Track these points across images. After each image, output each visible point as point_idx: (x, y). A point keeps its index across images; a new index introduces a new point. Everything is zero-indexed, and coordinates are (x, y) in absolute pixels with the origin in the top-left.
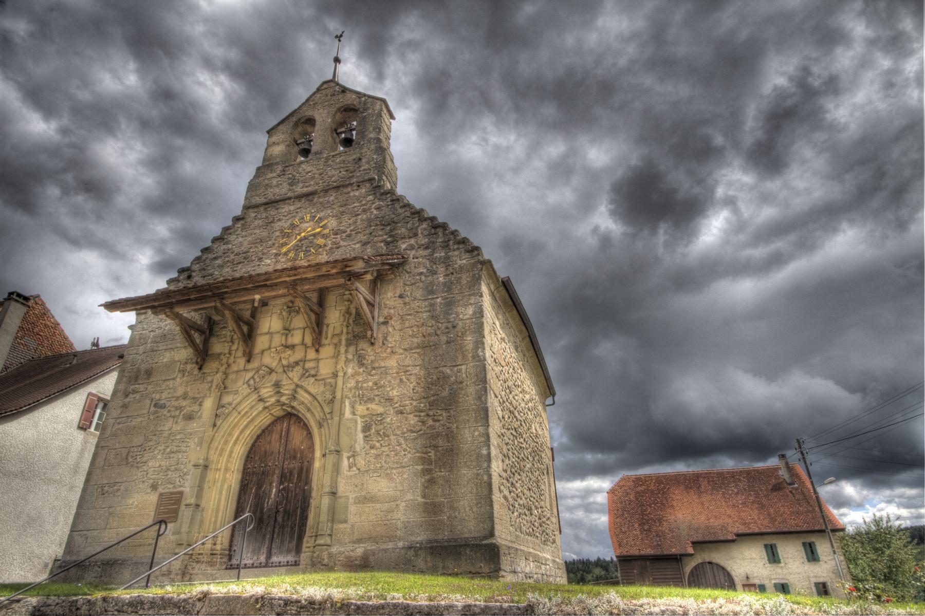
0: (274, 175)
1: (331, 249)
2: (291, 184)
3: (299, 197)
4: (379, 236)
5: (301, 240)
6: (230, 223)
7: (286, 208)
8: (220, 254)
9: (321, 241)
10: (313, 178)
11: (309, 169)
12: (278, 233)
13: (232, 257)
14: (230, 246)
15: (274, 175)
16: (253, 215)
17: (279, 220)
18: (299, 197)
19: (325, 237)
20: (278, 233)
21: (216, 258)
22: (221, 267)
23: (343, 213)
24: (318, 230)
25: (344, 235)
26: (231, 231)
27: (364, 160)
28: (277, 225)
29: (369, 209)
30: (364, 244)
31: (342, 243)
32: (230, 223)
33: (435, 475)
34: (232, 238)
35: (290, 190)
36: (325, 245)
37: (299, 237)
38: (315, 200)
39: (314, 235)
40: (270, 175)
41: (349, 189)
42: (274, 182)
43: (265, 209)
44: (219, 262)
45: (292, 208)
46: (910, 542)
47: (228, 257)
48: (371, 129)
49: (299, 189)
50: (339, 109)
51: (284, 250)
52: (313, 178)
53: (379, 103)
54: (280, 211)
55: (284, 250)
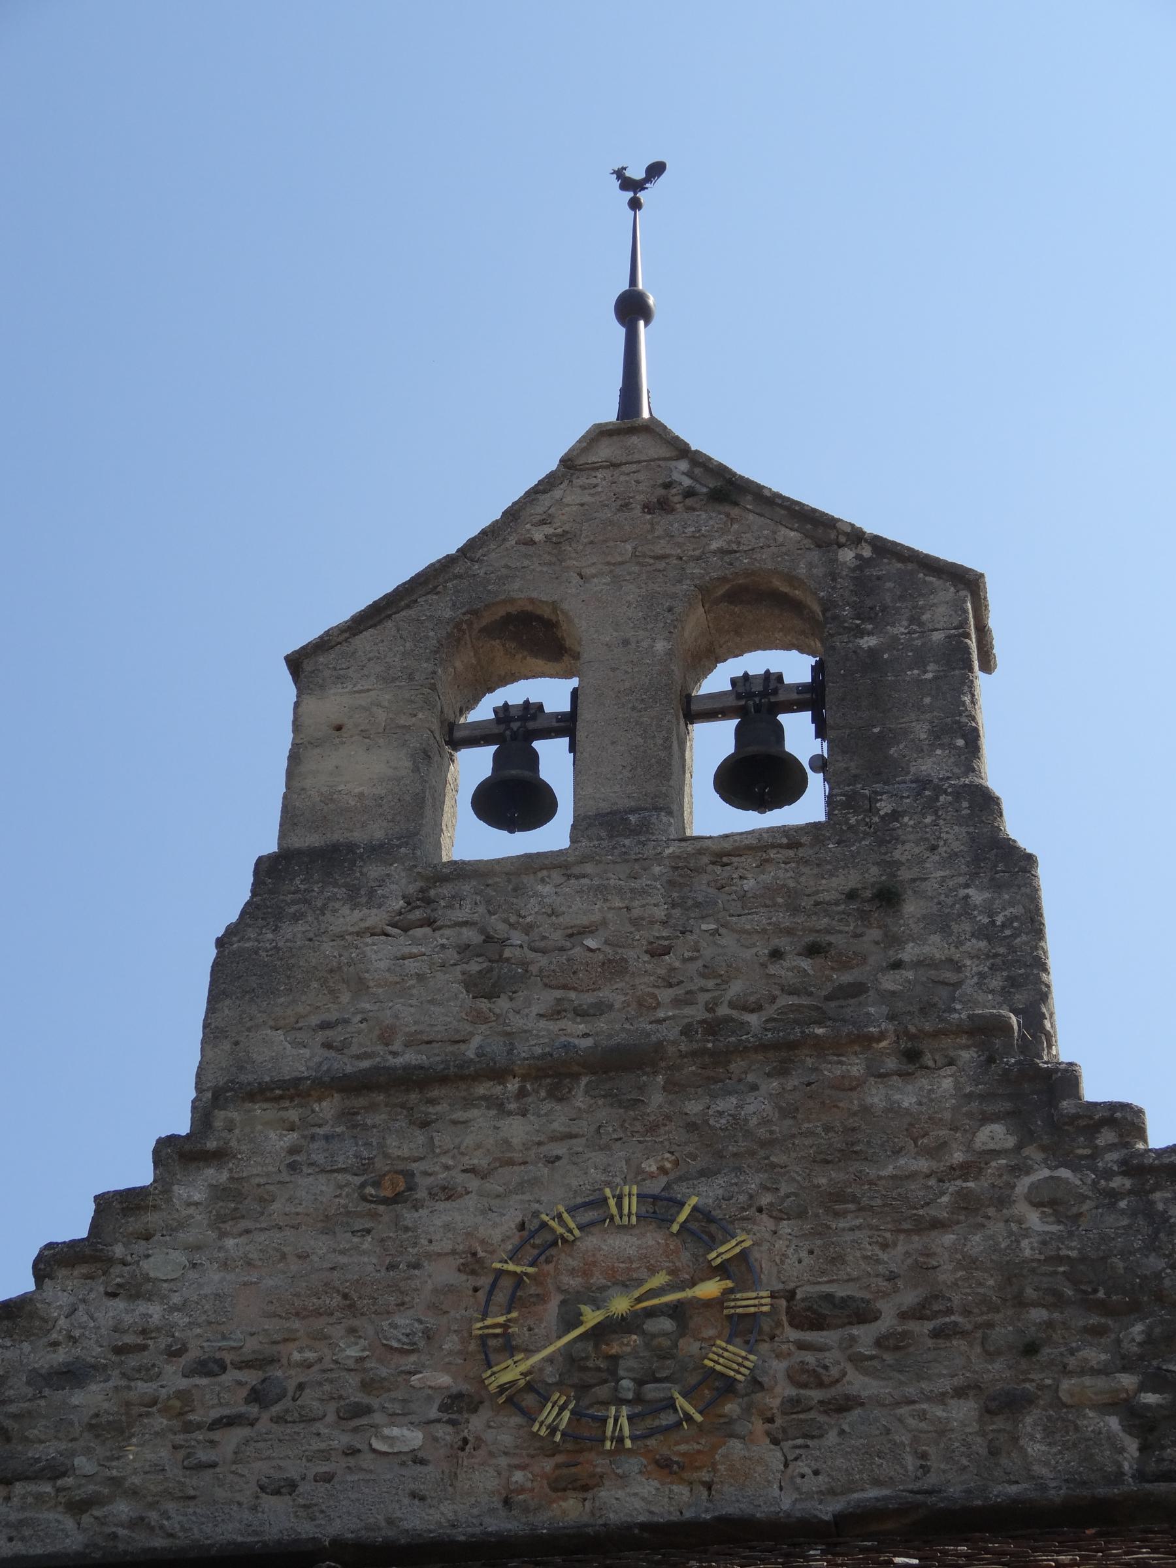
0: (376, 917)
1: (793, 1405)
2: (485, 987)
3: (555, 1074)
4: (1085, 1370)
5: (599, 1333)
6: (142, 1174)
7: (481, 1130)
8: (93, 1351)
9: (729, 1357)
10: (615, 968)
11: (579, 911)
12: (444, 1273)
13: (173, 1379)
14: (155, 1311)
15: (376, 917)
16: (279, 1141)
17: (448, 1193)
18: (555, 1074)
19: (744, 1328)
20: (444, 1273)
21: (72, 1375)
22: (110, 1430)
23: (835, 1199)
24: (710, 1289)
25: (865, 1334)
26: (152, 1219)
27: (911, 908)
28: (440, 1225)
29: (1002, 1201)
30: (1006, 1404)
31: (858, 1383)
32: (142, 1174)
33: (443, 1432)
34: (161, 1263)
35: (479, 1018)
36: (756, 1384)
37: (592, 1317)
38: (657, 1099)
39: (677, 1311)
40: (347, 918)
41: (856, 1067)
42: (379, 956)
43: (347, 1116)
44: (91, 1398)
45: (516, 1130)
46: (429, 1256)
47: (149, 1373)
48: (921, 731)
49: (533, 1022)
50: (704, 592)
51: (510, 1372)
52: (615, 968)
53: (946, 592)
54: (444, 1139)
55: (510, 1372)
